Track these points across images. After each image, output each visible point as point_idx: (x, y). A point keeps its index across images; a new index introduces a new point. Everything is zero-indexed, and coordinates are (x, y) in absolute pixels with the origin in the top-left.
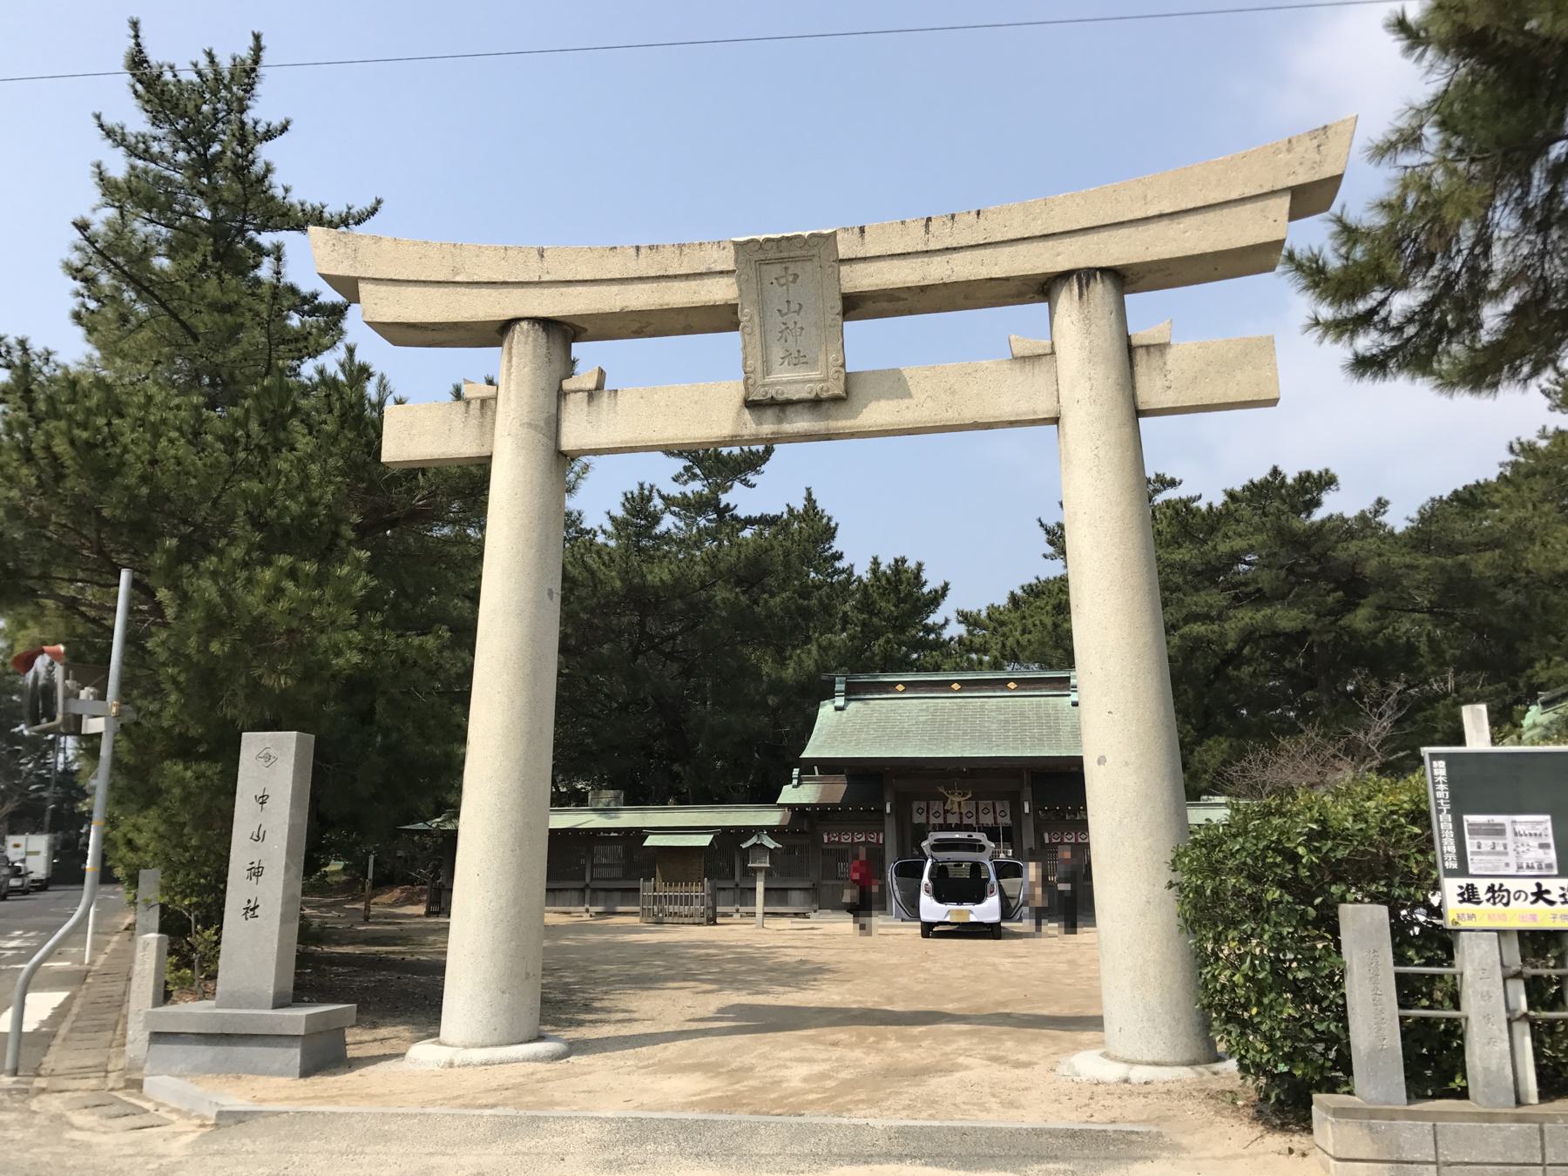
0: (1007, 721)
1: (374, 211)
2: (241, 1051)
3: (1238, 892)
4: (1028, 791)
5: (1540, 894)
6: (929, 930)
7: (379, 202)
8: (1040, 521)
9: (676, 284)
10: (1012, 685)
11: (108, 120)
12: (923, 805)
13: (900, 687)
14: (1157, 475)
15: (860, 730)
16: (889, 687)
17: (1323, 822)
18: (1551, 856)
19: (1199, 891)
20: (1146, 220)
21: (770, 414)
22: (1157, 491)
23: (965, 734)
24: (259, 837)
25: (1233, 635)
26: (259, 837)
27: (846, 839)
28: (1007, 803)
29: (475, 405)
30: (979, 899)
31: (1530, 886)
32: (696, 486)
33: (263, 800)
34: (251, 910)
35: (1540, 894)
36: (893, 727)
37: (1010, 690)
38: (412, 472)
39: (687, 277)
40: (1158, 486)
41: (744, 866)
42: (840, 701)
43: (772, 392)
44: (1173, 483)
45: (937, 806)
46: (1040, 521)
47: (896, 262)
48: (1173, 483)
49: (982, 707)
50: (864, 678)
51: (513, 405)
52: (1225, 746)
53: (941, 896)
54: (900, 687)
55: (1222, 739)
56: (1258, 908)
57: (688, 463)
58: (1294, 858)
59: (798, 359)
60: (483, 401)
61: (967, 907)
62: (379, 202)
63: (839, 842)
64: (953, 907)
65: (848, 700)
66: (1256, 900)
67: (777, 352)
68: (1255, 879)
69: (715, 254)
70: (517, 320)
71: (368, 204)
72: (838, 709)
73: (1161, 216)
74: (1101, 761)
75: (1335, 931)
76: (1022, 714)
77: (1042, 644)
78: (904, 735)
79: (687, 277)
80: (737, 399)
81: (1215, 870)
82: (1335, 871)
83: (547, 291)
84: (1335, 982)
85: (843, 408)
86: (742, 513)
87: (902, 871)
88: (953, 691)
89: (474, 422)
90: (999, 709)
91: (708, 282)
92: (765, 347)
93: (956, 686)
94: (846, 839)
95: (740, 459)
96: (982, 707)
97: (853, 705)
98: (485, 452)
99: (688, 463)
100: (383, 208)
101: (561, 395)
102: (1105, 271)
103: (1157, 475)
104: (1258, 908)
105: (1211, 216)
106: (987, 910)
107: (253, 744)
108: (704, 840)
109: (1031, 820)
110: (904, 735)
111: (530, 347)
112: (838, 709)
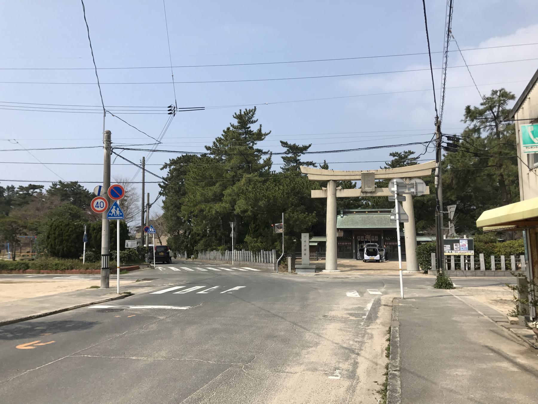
0: (378, 220)
1: (270, 133)
2: (307, 270)
3: (422, 252)
4: (383, 234)
5: (449, 252)
6: (365, 261)
7: (271, 131)
8: (380, 167)
9: (352, 176)
10: (379, 212)
11: (232, 124)
12: (360, 237)
13: (355, 212)
14: (409, 151)
15: (347, 222)
16: (352, 212)
17: (430, 246)
18: (450, 249)
19: (418, 252)
20: (414, 171)
21: (365, 193)
22: (409, 155)
23: (370, 223)
24: (305, 246)
25: (426, 200)
26: (305, 246)
27: (343, 244)
28: (377, 237)
29: (324, 191)
30: (376, 255)
31: (448, 251)
32: (290, 155)
33: (305, 242)
34: (305, 254)
35: (449, 252)
36: (354, 221)
37: (378, 213)
38: (313, 198)
39: (354, 175)
40: (409, 153)
41: (32, 243)
42: (342, 216)
43: (365, 191)
44: (413, 153)
45: (363, 237)
46: (380, 167)
47: (382, 175)
48: (413, 153)
49: (373, 217)
50: (347, 210)
51: (330, 191)
52: (424, 222)
53: (368, 254)
54: (355, 212)
55: (423, 221)
56: (424, 254)
57: (288, 149)
58: (427, 249)
59: (369, 187)
60: (325, 190)
61: (373, 257)
62: (271, 131)
63: (342, 244)
64: (370, 257)
65: (344, 215)
66: (424, 253)
67: (366, 186)
68: (424, 251)
69: (357, 173)
70: (330, 180)
71: (269, 132)
72: (341, 217)
73: (416, 171)
74: (407, 238)
75: (431, 255)
76: (381, 218)
77: (383, 201)
78: (357, 223)
79: (354, 175)
80: (360, 191)
81: (420, 250)
82: (430, 250)
83: (334, 176)
84: (431, 260)
85: (375, 193)
86: (301, 161)
87: (360, 250)
88: (366, 213)
89: (324, 193)
90: (376, 217)
91: (356, 176)
92: (365, 185)
93: (367, 212)
94: (343, 244)
95: (302, 148)
96: (373, 217)
97: (345, 216)
98: (326, 197)
99: (288, 149)
100: (271, 132)
101: (336, 190)
102: (408, 177)
103: (409, 151)
104: (424, 254)
105: (422, 171)
106: (377, 257)
107: (303, 235)
108: (316, 244)
109: (383, 240)
110: (357, 223)
111: (332, 184)
112: (341, 217)
